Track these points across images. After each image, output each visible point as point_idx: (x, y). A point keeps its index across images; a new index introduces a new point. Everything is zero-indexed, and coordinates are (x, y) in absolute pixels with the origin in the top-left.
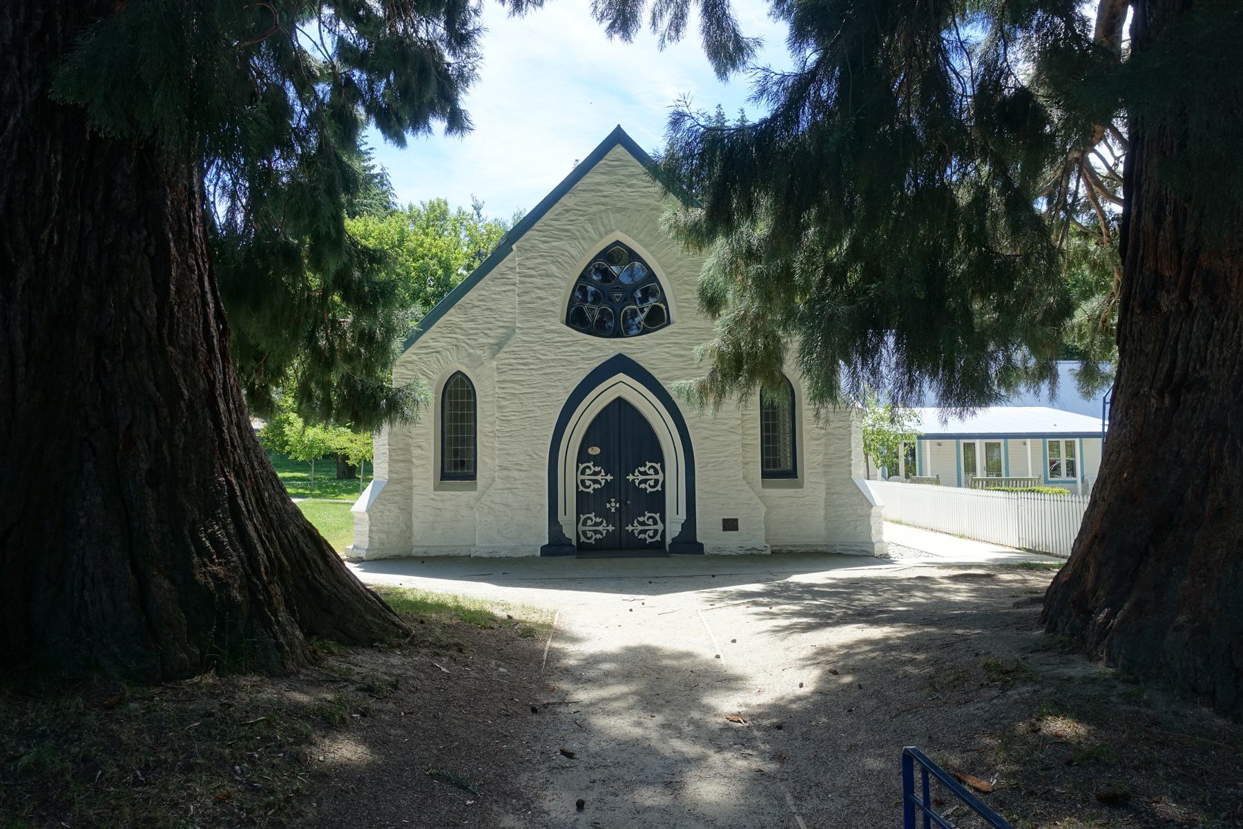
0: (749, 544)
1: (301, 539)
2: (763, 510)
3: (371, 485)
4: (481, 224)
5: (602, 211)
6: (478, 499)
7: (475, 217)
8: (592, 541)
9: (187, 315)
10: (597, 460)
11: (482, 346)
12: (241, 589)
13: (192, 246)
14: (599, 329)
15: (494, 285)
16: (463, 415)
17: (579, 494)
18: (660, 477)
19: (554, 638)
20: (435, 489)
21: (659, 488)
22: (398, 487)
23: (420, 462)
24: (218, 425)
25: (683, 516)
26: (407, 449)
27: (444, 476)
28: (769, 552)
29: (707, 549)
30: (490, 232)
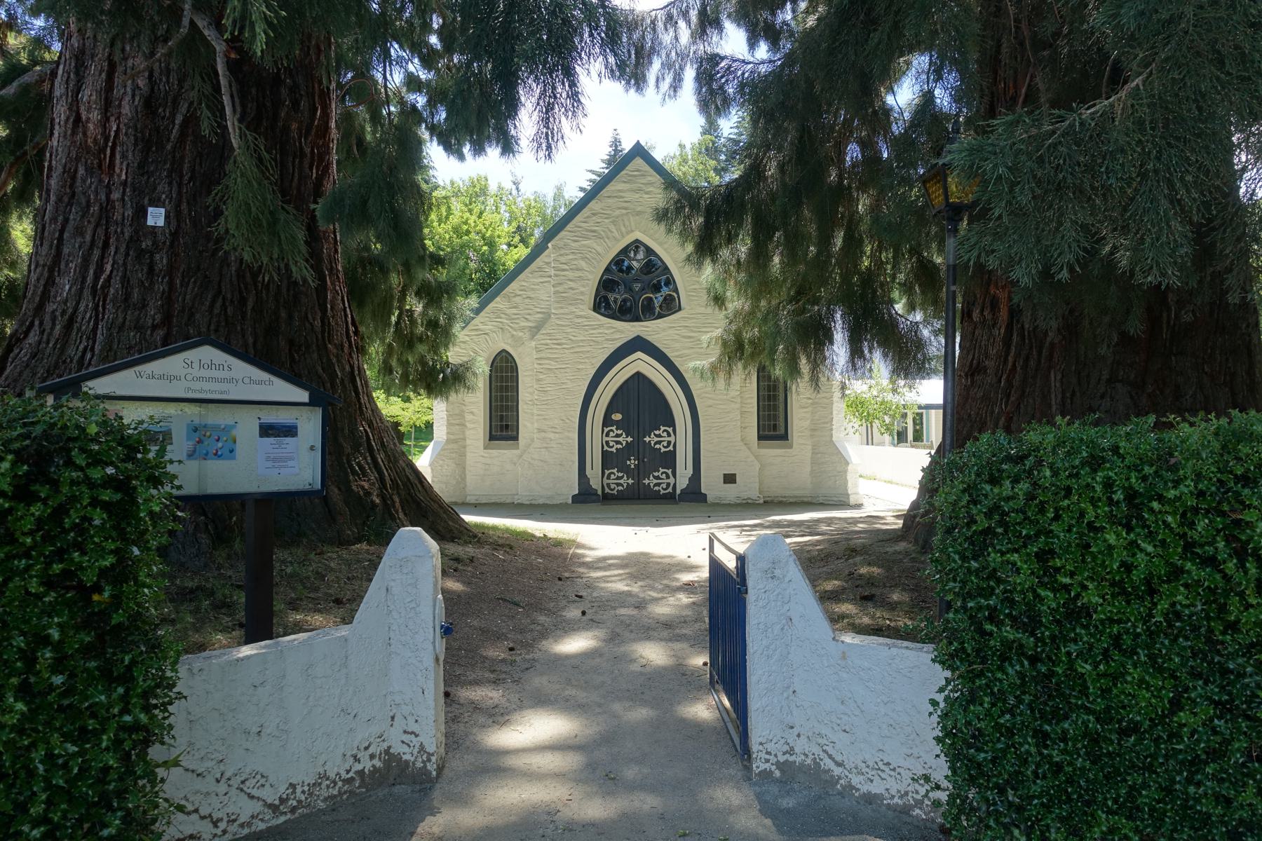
0: (745, 495)
1: (407, 469)
2: (757, 466)
3: (432, 444)
4: (520, 199)
5: (622, 215)
6: (521, 456)
7: (514, 192)
8: (615, 492)
9: (337, 324)
10: (619, 424)
11: (522, 329)
12: (378, 496)
13: (338, 277)
14: (625, 313)
15: (534, 277)
16: (501, 392)
17: (605, 455)
18: (672, 439)
19: (577, 548)
20: (485, 448)
21: (671, 448)
22: (454, 446)
23: (472, 426)
24: (357, 393)
25: (690, 471)
26: (461, 415)
27: (492, 438)
28: (762, 501)
29: (709, 499)
30: (529, 207)
